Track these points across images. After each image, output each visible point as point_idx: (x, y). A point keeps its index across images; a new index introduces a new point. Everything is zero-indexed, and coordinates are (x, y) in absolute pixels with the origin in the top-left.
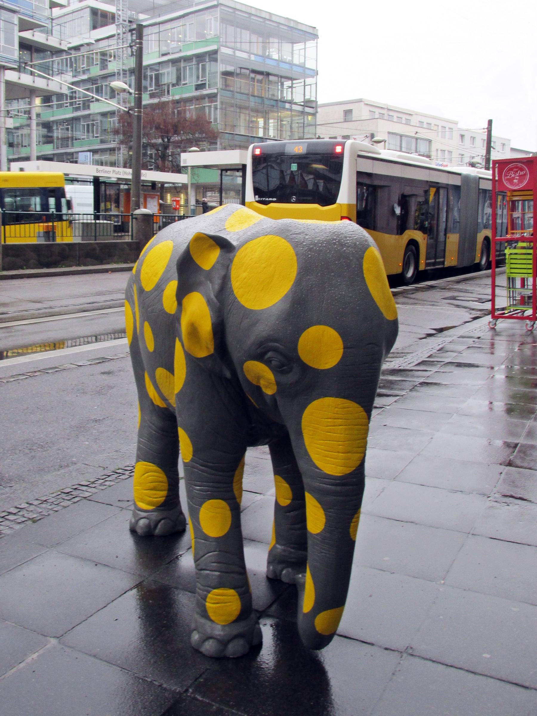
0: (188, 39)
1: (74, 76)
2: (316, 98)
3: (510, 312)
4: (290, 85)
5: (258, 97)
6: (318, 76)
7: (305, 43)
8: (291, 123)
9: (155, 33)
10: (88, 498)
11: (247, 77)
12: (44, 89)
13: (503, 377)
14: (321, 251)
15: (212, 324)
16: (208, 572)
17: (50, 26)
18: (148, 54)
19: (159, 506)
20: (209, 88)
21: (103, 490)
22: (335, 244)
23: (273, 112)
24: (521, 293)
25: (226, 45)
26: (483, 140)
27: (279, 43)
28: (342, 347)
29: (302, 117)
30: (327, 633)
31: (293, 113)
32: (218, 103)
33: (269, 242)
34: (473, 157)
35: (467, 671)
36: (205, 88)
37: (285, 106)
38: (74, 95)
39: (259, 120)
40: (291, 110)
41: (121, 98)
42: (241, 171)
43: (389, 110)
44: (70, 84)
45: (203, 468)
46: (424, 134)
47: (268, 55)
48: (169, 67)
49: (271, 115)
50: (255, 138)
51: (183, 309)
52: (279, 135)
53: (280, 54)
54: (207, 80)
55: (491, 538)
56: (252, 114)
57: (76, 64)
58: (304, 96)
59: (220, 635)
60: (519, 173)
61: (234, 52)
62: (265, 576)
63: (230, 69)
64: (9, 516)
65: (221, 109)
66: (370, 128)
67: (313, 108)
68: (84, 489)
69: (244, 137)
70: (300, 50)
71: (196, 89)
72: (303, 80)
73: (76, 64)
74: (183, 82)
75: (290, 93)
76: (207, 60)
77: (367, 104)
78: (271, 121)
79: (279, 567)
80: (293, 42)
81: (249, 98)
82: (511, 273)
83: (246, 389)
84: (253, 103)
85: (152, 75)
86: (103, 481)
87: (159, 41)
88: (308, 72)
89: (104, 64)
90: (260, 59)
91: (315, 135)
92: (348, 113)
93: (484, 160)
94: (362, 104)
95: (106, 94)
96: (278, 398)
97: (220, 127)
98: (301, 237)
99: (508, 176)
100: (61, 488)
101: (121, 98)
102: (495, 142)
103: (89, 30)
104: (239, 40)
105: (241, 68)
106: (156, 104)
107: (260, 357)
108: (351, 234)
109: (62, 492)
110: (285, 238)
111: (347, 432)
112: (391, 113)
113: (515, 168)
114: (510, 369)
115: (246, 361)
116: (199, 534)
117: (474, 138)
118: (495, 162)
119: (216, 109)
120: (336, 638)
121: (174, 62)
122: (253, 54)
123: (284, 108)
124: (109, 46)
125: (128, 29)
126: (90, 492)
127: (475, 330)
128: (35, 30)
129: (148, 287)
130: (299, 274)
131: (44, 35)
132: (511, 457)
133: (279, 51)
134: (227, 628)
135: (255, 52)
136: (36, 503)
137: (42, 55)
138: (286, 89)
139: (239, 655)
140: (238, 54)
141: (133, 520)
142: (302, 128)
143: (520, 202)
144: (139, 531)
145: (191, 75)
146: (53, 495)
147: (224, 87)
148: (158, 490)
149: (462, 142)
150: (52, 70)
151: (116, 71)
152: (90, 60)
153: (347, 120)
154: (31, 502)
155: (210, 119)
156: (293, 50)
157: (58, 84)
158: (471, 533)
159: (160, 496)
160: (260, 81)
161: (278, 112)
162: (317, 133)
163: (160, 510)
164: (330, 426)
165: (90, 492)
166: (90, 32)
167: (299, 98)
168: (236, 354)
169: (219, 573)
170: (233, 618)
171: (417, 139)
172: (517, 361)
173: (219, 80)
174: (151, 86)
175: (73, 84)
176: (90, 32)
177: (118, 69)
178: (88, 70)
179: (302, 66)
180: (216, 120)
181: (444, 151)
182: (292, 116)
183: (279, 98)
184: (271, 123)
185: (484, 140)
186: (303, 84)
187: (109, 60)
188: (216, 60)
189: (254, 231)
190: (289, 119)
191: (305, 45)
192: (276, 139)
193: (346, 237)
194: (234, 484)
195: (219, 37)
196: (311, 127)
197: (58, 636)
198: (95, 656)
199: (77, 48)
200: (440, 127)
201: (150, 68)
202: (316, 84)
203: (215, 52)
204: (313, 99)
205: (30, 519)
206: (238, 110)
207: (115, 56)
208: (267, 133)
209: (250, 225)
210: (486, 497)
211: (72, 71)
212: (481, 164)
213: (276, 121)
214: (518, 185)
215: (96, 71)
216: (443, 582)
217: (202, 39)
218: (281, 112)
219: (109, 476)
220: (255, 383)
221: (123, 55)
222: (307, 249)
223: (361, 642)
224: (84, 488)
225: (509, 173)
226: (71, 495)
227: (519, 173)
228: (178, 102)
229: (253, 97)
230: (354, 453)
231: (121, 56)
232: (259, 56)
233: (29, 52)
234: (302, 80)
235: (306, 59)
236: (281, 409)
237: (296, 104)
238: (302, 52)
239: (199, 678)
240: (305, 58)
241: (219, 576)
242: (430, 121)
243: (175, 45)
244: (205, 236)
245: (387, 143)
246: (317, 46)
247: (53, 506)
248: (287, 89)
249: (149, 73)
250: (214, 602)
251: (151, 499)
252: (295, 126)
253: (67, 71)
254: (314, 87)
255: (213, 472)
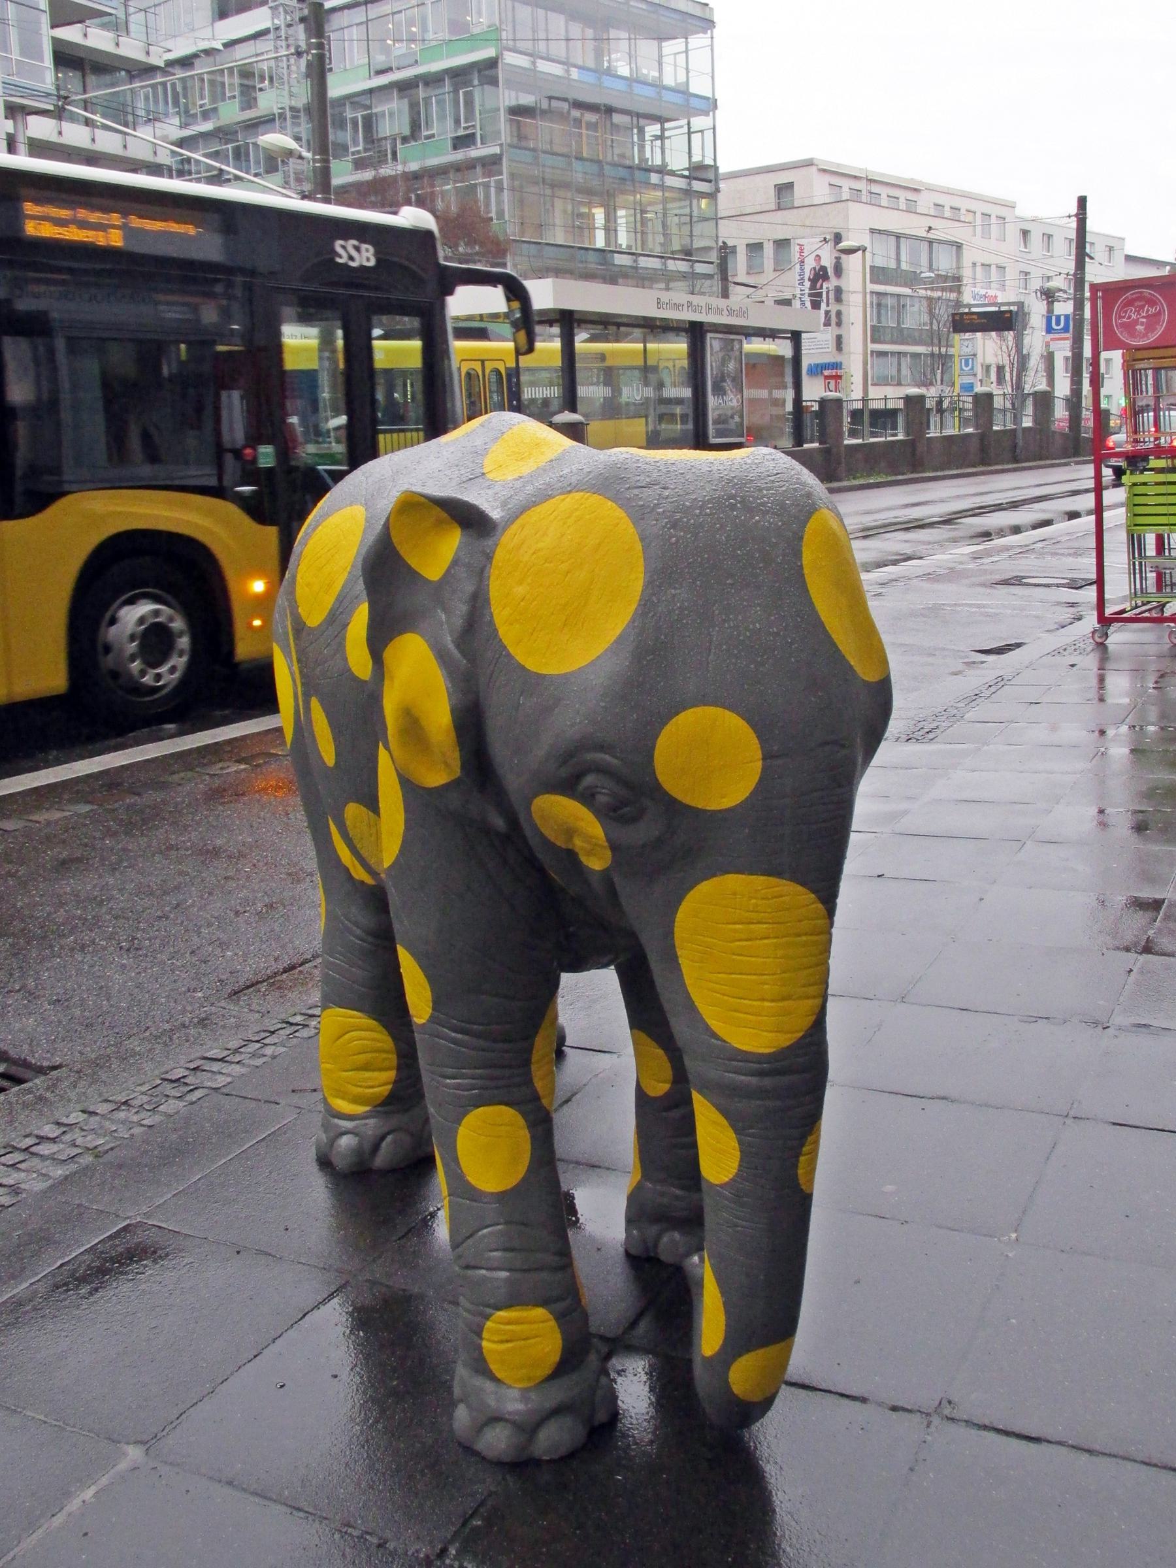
0: (430, 35)
1: (183, 126)
2: (715, 160)
3: (1137, 607)
4: (659, 133)
5: (591, 161)
6: (717, 111)
7: (687, 38)
8: (665, 215)
9: (358, 25)
10: (224, 1090)
11: (563, 117)
12: (117, 156)
13: (1125, 751)
14: (701, 525)
15: (453, 711)
16: (483, 1272)
17: (121, 15)
18: (346, 70)
19: (379, 1105)
20: (482, 144)
21: (257, 1067)
22: (733, 507)
23: (623, 192)
24: (1157, 567)
25: (515, 46)
26: (1067, 241)
27: (630, 39)
28: (759, 754)
29: (688, 203)
30: (757, 1397)
31: (667, 194)
32: (505, 177)
33: (576, 510)
34: (1049, 279)
35: (1073, 1447)
36: (474, 143)
37: (649, 178)
38: (186, 167)
39: (594, 211)
40: (662, 187)
41: (291, 171)
42: (558, 324)
43: (871, 181)
44: (172, 144)
45: (460, 1036)
46: (945, 230)
47: (609, 67)
48: (392, 99)
49: (620, 199)
50: (590, 252)
51: (386, 676)
52: (639, 243)
53: (633, 66)
54: (478, 127)
55: (1114, 1124)
56: (579, 198)
57: (185, 97)
58: (690, 157)
59: (517, 1412)
60: (1148, 311)
61: (534, 63)
62: (621, 1250)
63: (527, 100)
64: (40, 1147)
65: (512, 189)
66: (834, 222)
67: (710, 181)
68: (214, 1069)
69: (562, 250)
70: (675, 54)
71: (455, 148)
72: (685, 121)
73: (185, 97)
74: (425, 133)
75: (658, 151)
76: (476, 82)
77: (824, 171)
78: (621, 213)
79: (653, 1230)
80: (662, 38)
81: (570, 164)
82: (1136, 525)
83: (541, 855)
84: (580, 175)
85: (356, 117)
86: (258, 1045)
87: (368, 40)
88: (694, 103)
89: (248, 97)
90: (590, 78)
91: (717, 241)
92: (784, 189)
93: (1072, 283)
94: (814, 169)
95: (258, 163)
96: (617, 879)
97: (510, 229)
98: (650, 495)
99: (1124, 317)
100: (163, 1070)
101: (291, 171)
102: (1092, 244)
103: (210, 20)
104: (542, 35)
105: (550, 98)
106: (368, 183)
107: (568, 786)
108: (773, 482)
109: (163, 1079)
110: (615, 500)
111: (780, 953)
112: (875, 188)
113: (1138, 299)
114: (1137, 729)
115: (536, 795)
116: (461, 1188)
117: (1050, 236)
118: (1094, 288)
119: (500, 189)
120: (785, 1391)
121: (404, 87)
122: (575, 66)
123: (648, 184)
124: (257, 55)
125: (297, 16)
126: (229, 1075)
127: (1065, 650)
128: (88, 22)
129: (314, 618)
130: (648, 584)
131: (110, 35)
132: (1151, 933)
133: (632, 57)
134: (533, 1396)
135: (580, 63)
136: (103, 1108)
137: (107, 78)
138: (649, 143)
139: (563, 1451)
140: (544, 66)
141: (324, 1137)
142: (689, 226)
143: (1150, 372)
144: (340, 1163)
145: (442, 118)
146: (144, 1088)
147: (515, 140)
148: (374, 1070)
149: (1026, 247)
150: (133, 114)
151: (276, 111)
152: (218, 92)
153: (782, 207)
154: (91, 1109)
155: (489, 212)
156: (660, 56)
157: (150, 146)
158: (1072, 1113)
159: (381, 1081)
160: (592, 126)
161: (634, 193)
162: (720, 235)
163: (378, 1112)
164: (740, 940)
165: (229, 1075)
166: (212, 24)
167: (678, 162)
168: (513, 780)
169: (508, 1274)
170: (547, 1371)
171: (931, 242)
172: (1153, 713)
173: (503, 124)
174: (356, 143)
175: (181, 143)
176: (212, 24)
177: (280, 106)
178: (215, 110)
179: (683, 91)
180: (500, 214)
181: (989, 266)
182: (665, 201)
183: (637, 162)
184: (621, 217)
185: (1071, 240)
186: (685, 129)
187: (259, 86)
188: (494, 82)
189: (539, 483)
190: (659, 208)
191: (687, 43)
192: (634, 251)
193: (760, 490)
194: (534, 1067)
195: (498, 30)
196: (706, 223)
197: (145, 1437)
198: (230, 1483)
199: (186, 62)
200: (978, 215)
201: (351, 103)
202: (714, 128)
203: (492, 63)
204: (709, 161)
205: (88, 1149)
206: (548, 192)
207: (271, 79)
208: (613, 240)
209: (541, 464)
210: (1100, 1028)
211: (178, 113)
212: (1065, 292)
213: (632, 212)
214: (1145, 335)
215: (231, 112)
216: (1014, 1235)
217: (461, 33)
218: (640, 193)
219: (273, 1033)
220: (560, 843)
221: (289, 75)
222: (667, 523)
223: (837, 1396)
224: (216, 1067)
225: (1126, 312)
226: (186, 1084)
227: (1148, 311)
228: (416, 176)
229: (580, 163)
230: (800, 998)
231: (285, 77)
232: (589, 70)
233: (79, 74)
234: (684, 122)
235: (690, 75)
236: (623, 901)
237: (672, 173)
238: (681, 59)
239: (472, 1516)
240: (688, 72)
241: (507, 1280)
242: (957, 202)
243: (404, 51)
244: (423, 499)
245: (867, 254)
246: (712, 46)
247: (143, 1115)
248: (652, 141)
249: (349, 114)
250: (504, 1338)
251: (360, 1090)
252: (673, 221)
253: (166, 115)
254: (709, 135)
255: (481, 1043)
